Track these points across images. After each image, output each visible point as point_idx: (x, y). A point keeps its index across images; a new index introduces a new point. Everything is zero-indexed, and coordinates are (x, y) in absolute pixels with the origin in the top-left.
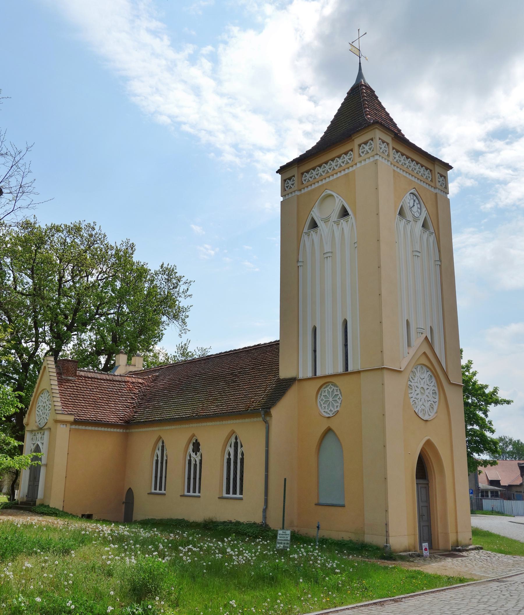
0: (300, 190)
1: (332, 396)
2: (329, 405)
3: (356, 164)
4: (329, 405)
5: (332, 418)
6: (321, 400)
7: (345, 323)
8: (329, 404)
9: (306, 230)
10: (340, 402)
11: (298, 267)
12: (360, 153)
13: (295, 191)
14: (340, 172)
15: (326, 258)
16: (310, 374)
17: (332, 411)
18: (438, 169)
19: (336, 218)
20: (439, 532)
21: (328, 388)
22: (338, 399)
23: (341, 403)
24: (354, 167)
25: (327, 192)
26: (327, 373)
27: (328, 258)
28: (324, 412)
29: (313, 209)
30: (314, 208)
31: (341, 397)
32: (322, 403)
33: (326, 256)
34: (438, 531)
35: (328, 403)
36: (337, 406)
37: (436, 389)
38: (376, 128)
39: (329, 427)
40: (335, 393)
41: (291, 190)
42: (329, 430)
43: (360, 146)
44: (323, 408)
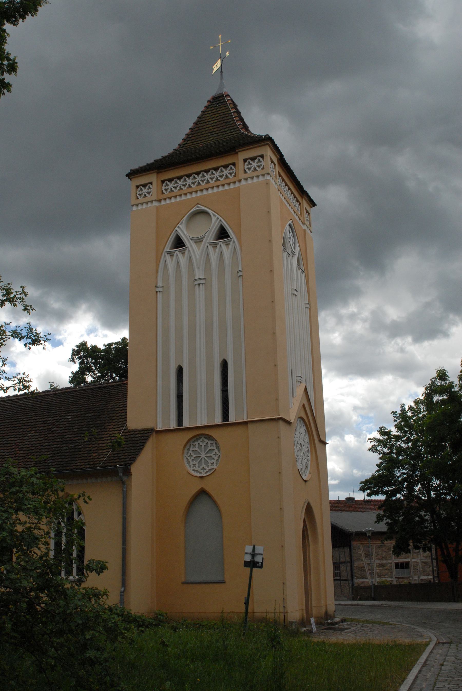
0: (160, 201)
1: (204, 451)
2: (200, 462)
3: (240, 181)
4: (200, 462)
5: (207, 477)
6: (189, 456)
7: (224, 364)
8: (201, 460)
9: (168, 249)
10: (216, 458)
11: (157, 292)
12: (163, 190)
13: (152, 202)
14: (170, 198)
15: (197, 285)
16: (173, 425)
17: (205, 469)
18: (305, 205)
19: (212, 239)
20: (313, 606)
21: (199, 442)
22: (214, 454)
23: (217, 460)
24: (237, 185)
25: (198, 207)
26: (199, 424)
27: (201, 285)
28: (193, 470)
29: (179, 225)
30: (181, 224)
31: (218, 453)
32: (190, 460)
33: (196, 282)
34: (311, 604)
35: (199, 460)
36: (212, 464)
37: (309, 446)
38: (268, 144)
39: (202, 488)
40: (209, 448)
41: (146, 200)
42: (203, 493)
43: (245, 161)
44: (192, 466)
